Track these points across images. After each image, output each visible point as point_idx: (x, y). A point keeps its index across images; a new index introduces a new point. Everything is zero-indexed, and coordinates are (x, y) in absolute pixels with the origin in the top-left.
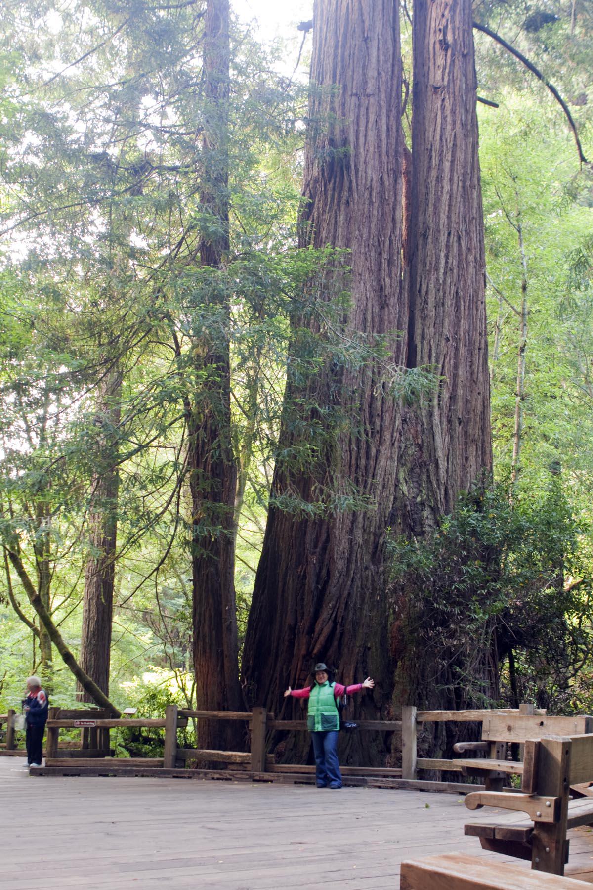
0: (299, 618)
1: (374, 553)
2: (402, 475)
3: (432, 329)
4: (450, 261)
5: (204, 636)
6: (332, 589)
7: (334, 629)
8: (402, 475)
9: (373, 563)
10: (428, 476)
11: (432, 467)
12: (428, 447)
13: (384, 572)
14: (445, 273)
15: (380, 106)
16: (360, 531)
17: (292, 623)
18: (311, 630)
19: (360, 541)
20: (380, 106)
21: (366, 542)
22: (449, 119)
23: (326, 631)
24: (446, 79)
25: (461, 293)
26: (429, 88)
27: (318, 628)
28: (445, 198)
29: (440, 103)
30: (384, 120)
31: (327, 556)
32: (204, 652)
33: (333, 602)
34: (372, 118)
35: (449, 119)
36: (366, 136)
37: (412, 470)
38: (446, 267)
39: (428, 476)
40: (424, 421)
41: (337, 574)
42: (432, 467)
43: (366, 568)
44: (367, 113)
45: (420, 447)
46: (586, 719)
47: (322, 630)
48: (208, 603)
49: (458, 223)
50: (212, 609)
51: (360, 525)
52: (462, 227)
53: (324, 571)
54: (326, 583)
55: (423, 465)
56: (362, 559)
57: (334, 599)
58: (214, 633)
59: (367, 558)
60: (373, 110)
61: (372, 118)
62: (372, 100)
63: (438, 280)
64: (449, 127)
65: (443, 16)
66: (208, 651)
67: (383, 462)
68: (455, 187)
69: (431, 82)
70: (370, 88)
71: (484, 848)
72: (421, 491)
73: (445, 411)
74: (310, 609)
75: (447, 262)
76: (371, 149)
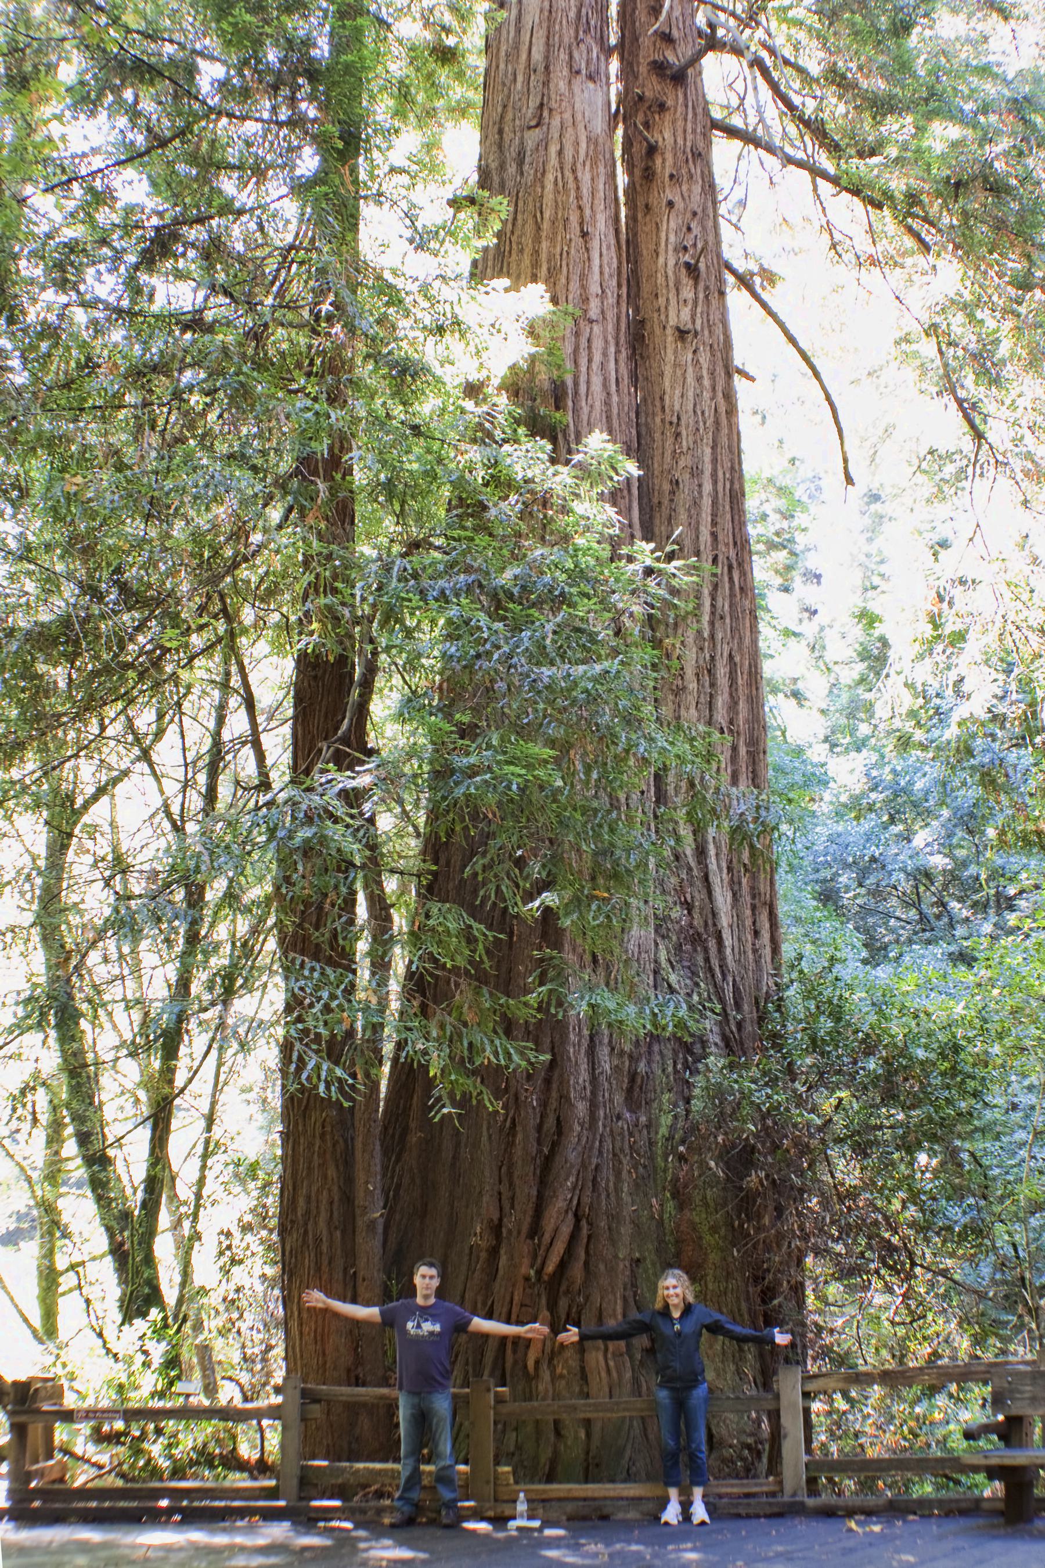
0: (506, 1205)
1: (630, 1091)
2: (663, 956)
3: (693, 711)
4: (719, 604)
5: (318, 1241)
6: (571, 1154)
7: (577, 1227)
8: (663, 956)
9: (631, 1111)
10: (707, 960)
11: (712, 944)
12: (702, 909)
13: (648, 1127)
14: (712, 623)
15: (606, 342)
16: (606, 1050)
17: (495, 1217)
18: (535, 1230)
19: (607, 1067)
20: (606, 342)
21: (616, 1069)
22: (706, 382)
23: (566, 1230)
24: (698, 322)
25: (737, 659)
26: (669, 331)
27: (549, 1224)
28: (706, 502)
29: (690, 356)
30: (612, 365)
31: (554, 1094)
32: (318, 1269)
33: (572, 1179)
34: (597, 358)
35: (706, 382)
36: (588, 382)
37: (679, 947)
38: (713, 613)
39: (707, 960)
40: (693, 864)
41: (577, 1128)
42: (712, 944)
43: (619, 1117)
44: (589, 347)
45: (689, 907)
46: (455, 1396)
47: (556, 1230)
48: (325, 1177)
49: (727, 545)
50: (335, 1189)
51: (606, 1041)
52: (732, 554)
53: (550, 1122)
54: (555, 1146)
55: (696, 940)
56: (611, 1100)
57: (574, 1172)
58: (338, 1233)
59: (619, 1098)
60: (598, 344)
61: (597, 358)
62: (596, 328)
63: (699, 632)
64: (706, 395)
65: (689, 229)
66: (325, 1267)
67: (635, 931)
68: (720, 485)
69: (673, 321)
70: (594, 312)
71: (18, 1528)
72: (697, 985)
73: (725, 850)
74: (527, 1190)
75: (713, 606)
76: (598, 404)
